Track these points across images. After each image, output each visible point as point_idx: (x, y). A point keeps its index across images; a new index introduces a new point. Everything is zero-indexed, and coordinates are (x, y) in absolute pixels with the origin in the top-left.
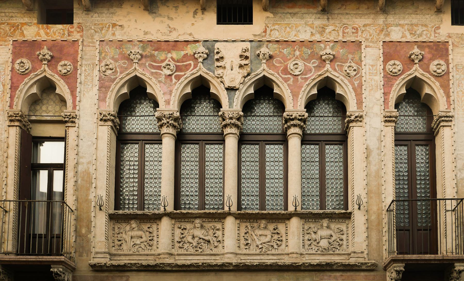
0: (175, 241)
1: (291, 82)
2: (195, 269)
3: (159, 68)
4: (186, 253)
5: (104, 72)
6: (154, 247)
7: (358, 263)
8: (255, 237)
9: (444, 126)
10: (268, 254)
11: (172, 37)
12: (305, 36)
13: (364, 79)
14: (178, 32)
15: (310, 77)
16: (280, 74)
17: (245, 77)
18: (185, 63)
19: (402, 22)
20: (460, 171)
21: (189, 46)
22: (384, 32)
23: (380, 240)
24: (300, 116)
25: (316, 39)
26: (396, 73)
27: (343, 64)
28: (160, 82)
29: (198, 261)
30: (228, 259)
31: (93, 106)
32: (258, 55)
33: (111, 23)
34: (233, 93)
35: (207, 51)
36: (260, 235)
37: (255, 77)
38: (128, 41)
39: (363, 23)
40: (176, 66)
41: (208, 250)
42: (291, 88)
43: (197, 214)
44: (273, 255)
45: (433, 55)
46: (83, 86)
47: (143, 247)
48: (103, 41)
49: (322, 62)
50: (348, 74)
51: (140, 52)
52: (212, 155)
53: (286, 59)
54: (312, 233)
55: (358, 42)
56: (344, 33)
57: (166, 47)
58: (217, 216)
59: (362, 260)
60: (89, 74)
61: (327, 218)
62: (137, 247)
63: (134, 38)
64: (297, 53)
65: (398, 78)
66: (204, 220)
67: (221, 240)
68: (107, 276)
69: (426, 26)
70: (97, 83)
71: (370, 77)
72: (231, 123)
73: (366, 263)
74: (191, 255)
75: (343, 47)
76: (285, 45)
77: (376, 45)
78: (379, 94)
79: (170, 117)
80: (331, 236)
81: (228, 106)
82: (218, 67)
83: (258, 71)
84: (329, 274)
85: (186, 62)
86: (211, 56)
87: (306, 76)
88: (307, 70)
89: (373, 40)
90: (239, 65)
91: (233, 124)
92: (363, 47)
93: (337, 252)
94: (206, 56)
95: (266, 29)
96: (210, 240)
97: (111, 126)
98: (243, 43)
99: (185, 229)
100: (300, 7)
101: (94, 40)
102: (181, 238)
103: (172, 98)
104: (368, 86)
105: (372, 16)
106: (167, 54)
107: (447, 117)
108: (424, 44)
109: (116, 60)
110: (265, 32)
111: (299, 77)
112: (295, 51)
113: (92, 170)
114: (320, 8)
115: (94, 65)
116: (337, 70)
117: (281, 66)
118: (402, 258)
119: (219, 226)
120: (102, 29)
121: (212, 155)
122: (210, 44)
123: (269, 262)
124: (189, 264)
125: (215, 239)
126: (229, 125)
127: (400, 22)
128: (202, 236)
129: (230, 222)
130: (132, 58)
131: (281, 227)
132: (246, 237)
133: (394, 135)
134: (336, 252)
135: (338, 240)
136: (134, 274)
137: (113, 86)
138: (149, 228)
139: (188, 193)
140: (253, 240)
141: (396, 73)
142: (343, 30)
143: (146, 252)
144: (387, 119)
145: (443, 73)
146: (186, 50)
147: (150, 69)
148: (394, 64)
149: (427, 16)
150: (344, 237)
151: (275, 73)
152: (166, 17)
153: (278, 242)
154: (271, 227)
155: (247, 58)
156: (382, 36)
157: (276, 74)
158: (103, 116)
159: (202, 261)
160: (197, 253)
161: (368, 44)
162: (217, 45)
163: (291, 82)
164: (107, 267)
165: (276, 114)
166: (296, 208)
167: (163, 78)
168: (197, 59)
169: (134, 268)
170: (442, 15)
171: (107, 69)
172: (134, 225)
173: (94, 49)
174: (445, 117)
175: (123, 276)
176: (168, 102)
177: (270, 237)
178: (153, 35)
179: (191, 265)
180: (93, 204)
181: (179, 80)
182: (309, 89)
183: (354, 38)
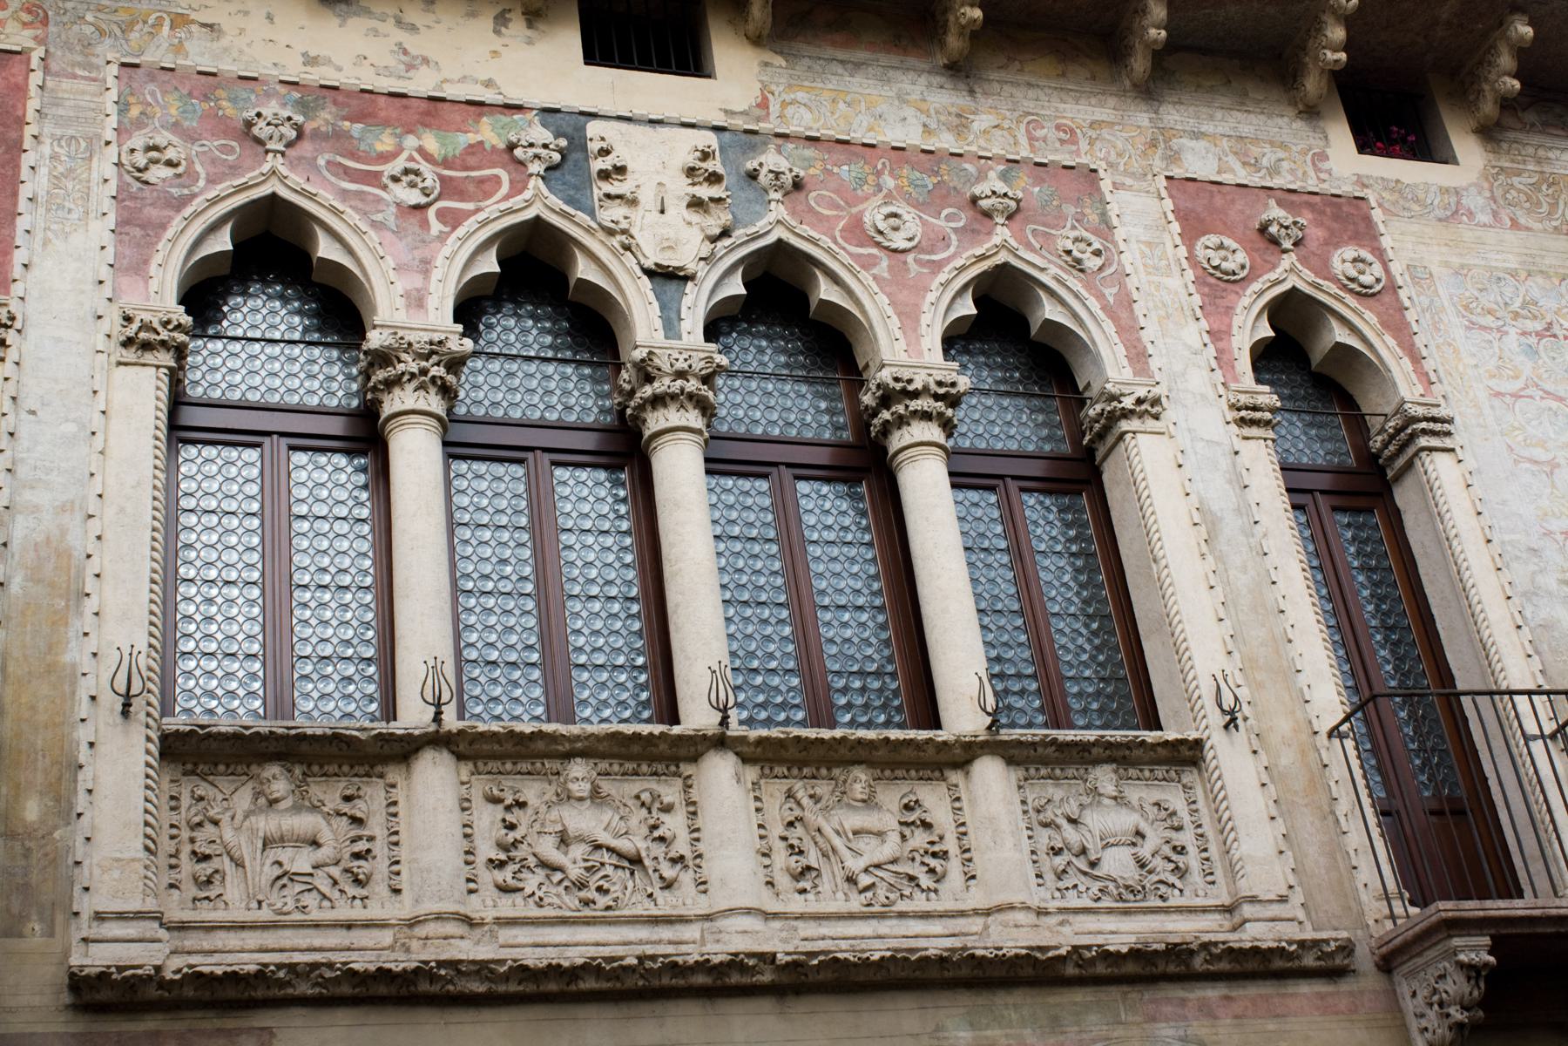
2: (605, 985)
3: (373, 178)
4: (535, 912)
5: (139, 170)
6: (380, 888)
7: (1290, 943)
8: (838, 842)
9: (1431, 450)
10: (902, 915)
11: (421, 84)
12: (911, 136)
14: (439, 70)
15: (948, 260)
16: (840, 240)
17: (714, 240)
19: (1207, 127)
20: (1529, 600)
21: (485, 119)
22: (1160, 151)
23: (1335, 850)
24: (940, 384)
26: (1234, 273)
29: (619, 951)
31: (90, 287)
33: (169, 13)
34: (672, 287)
35: (563, 143)
36: (855, 833)
39: (1090, 118)
40: (442, 179)
41: (638, 897)
43: (578, 738)
45: (1332, 232)
46: (41, 211)
48: (136, 66)
49: (979, 217)
50: (1078, 261)
51: (299, 119)
55: (1086, 171)
56: (1031, 139)
59: (1292, 932)
60: (71, 170)
62: (298, 888)
63: (262, 66)
65: (1244, 290)
66: (603, 765)
67: (688, 855)
69: (1283, 146)
71: (1152, 278)
72: (682, 390)
73: (1316, 943)
74: (563, 922)
75: (1039, 181)
76: (839, 153)
78: (1194, 333)
79: (433, 352)
80: (1139, 834)
82: (608, 196)
83: (761, 225)
84: (1176, 992)
86: (573, 155)
87: (934, 257)
90: (688, 199)
91: (691, 396)
94: (557, 157)
95: (765, 99)
96: (643, 854)
97: (169, 368)
98: (690, 131)
99: (522, 805)
100: (871, 47)
101: (94, 60)
102: (502, 846)
104: (1151, 305)
105: (1112, 101)
106: (400, 136)
107: (1434, 420)
108: (1294, 197)
109: (191, 137)
110: (764, 104)
111: (910, 258)
112: (879, 174)
113: (79, 540)
114: (942, 60)
115: (95, 144)
117: (838, 218)
118: (1481, 913)
119: (670, 792)
120: (126, 28)
122: (570, 126)
123: (934, 947)
124: (580, 961)
125: (658, 850)
126: (674, 397)
127: (1204, 128)
128: (605, 838)
130: (262, 136)
131: (934, 799)
134: (1172, 902)
135: (1167, 850)
137: (177, 223)
138: (348, 799)
139: (494, 655)
141: (1234, 273)
142: (1027, 131)
143: (344, 912)
144: (1243, 413)
145: (1378, 288)
146: (477, 132)
147: (333, 179)
148: (1221, 247)
149: (1280, 121)
150: (1187, 838)
152: (393, 21)
153: (933, 863)
154: (891, 797)
155: (714, 178)
156: (1158, 164)
157: (826, 241)
158: (140, 329)
159: (639, 950)
160: (587, 912)
161: (1119, 179)
162: (593, 128)
164: (163, 984)
166: (438, 714)
167: (389, 215)
168: (521, 163)
170: (1321, 124)
171: (156, 162)
172: (280, 787)
174: (1427, 419)
175: (239, 1031)
178: (340, 69)
180: (85, 688)
181: (454, 228)
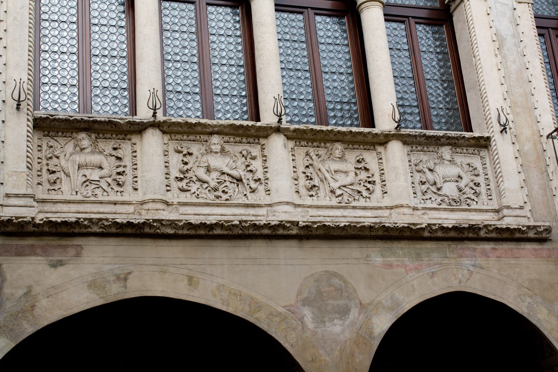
2: (225, 232)
4: (195, 200)
7: (523, 226)
8: (328, 175)
10: (354, 208)
29: (231, 218)
30: (286, 214)
36: (335, 172)
41: (240, 195)
43: (215, 126)
58: (253, 131)
59: (525, 222)
61: (449, 144)
62: (94, 186)
66: (226, 138)
67: (262, 178)
68: (32, 246)
73: (535, 227)
74: (208, 205)
80: (460, 177)
84: (472, 245)
96: (243, 177)
99: (190, 154)
119: (255, 151)
123: (367, 222)
124: (214, 222)
125: (249, 175)
129: (277, 145)
133: (533, 20)
135: (472, 184)
136: (93, 241)
138: (115, 149)
139: (180, 89)
140: (323, 180)
143: (113, 197)
150: (481, 179)
153: (369, 186)
154: (352, 156)
159: (240, 218)
160: (218, 201)
164: (36, 225)
169: (96, 229)
172: (86, 143)
175: (67, 246)
177: (353, 174)
179: (217, 225)
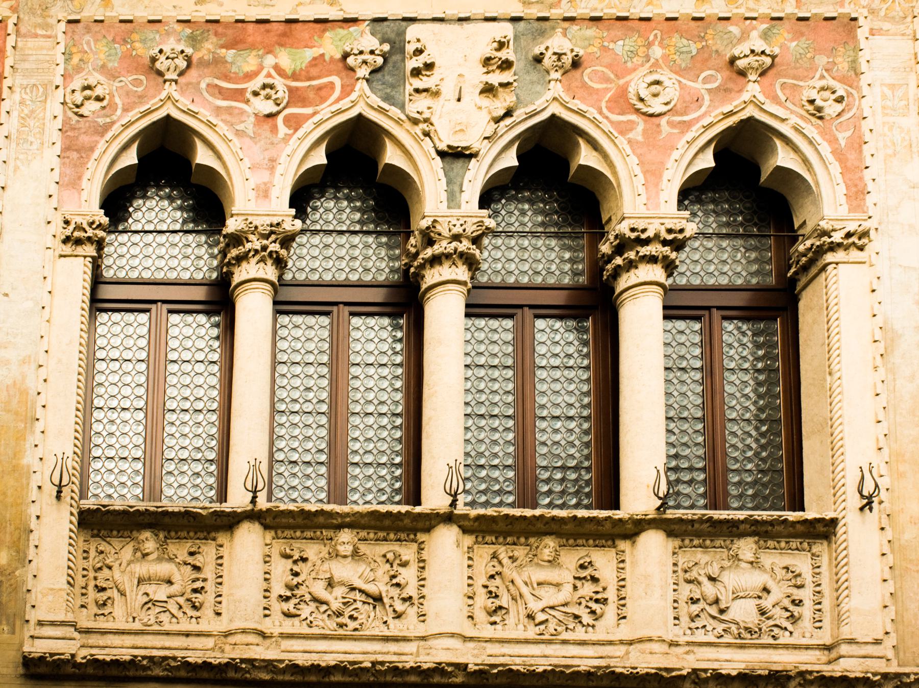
0: (274, 595)
1: (637, 134)
3: (238, 95)
4: (306, 630)
5: (78, 106)
7: (874, 674)
8: (525, 590)
10: (565, 642)
13: (865, 126)
15: (697, 120)
16: (605, 111)
17: (498, 120)
18: (314, 83)
21: (327, 34)
24: (670, 231)
25: (716, 11)
27: (801, 83)
28: (239, 133)
29: (359, 658)
32: (538, 59)
34: (458, 165)
36: (539, 584)
37: (526, 119)
38: (150, 22)
42: (639, 151)
43: (347, 515)
44: (583, 643)
46: (13, 145)
47: (173, 611)
49: (734, 75)
50: (819, 109)
51: (189, 51)
52: (371, 347)
53: (621, 70)
54: (704, 580)
55: (846, 20)
57: (259, 39)
60: (32, 112)
62: (158, 610)
64: (657, 52)
66: (363, 534)
70: (57, 137)
72: (456, 250)
75: (798, 35)
77: (902, 27)
79: (272, 232)
80: (766, 590)
81: (445, 203)
82: (417, 91)
83: (539, 104)
85: (319, 77)
87: (686, 118)
88: (688, 98)
89: (894, 14)
91: (462, 255)
92: (861, 33)
93: (785, 638)
94: (380, 60)
96: (384, 595)
97: (92, 257)
99: (304, 560)
101: (50, 20)
102: (289, 587)
103: (277, 179)
106: (261, 57)
109: (113, 76)
111: (663, 121)
112: (649, 45)
116: (783, 98)
117: (607, 90)
119: (408, 552)
121: (371, 347)
124: (333, 663)
125: (395, 592)
131: (604, 561)
132: (494, 589)
135: (787, 603)
137: (101, 146)
138: (192, 554)
143: (185, 626)
146: (320, 46)
147: (210, 99)
151: (591, 109)
154: (571, 558)
155: (506, 65)
159: (373, 658)
160: (341, 632)
161: (877, 25)
162: (412, 32)
163: (637, 134)
164: (76, 665)
165: (372, 227)
167: (249, 125)
168: (352, 69)
169: (158, 672)
171: (88, 98)
173: (49, 43)
176: (264, 192)
177: (570, 588)
181: (296, 130)
182: (300, 150)
183: (831, 8)
